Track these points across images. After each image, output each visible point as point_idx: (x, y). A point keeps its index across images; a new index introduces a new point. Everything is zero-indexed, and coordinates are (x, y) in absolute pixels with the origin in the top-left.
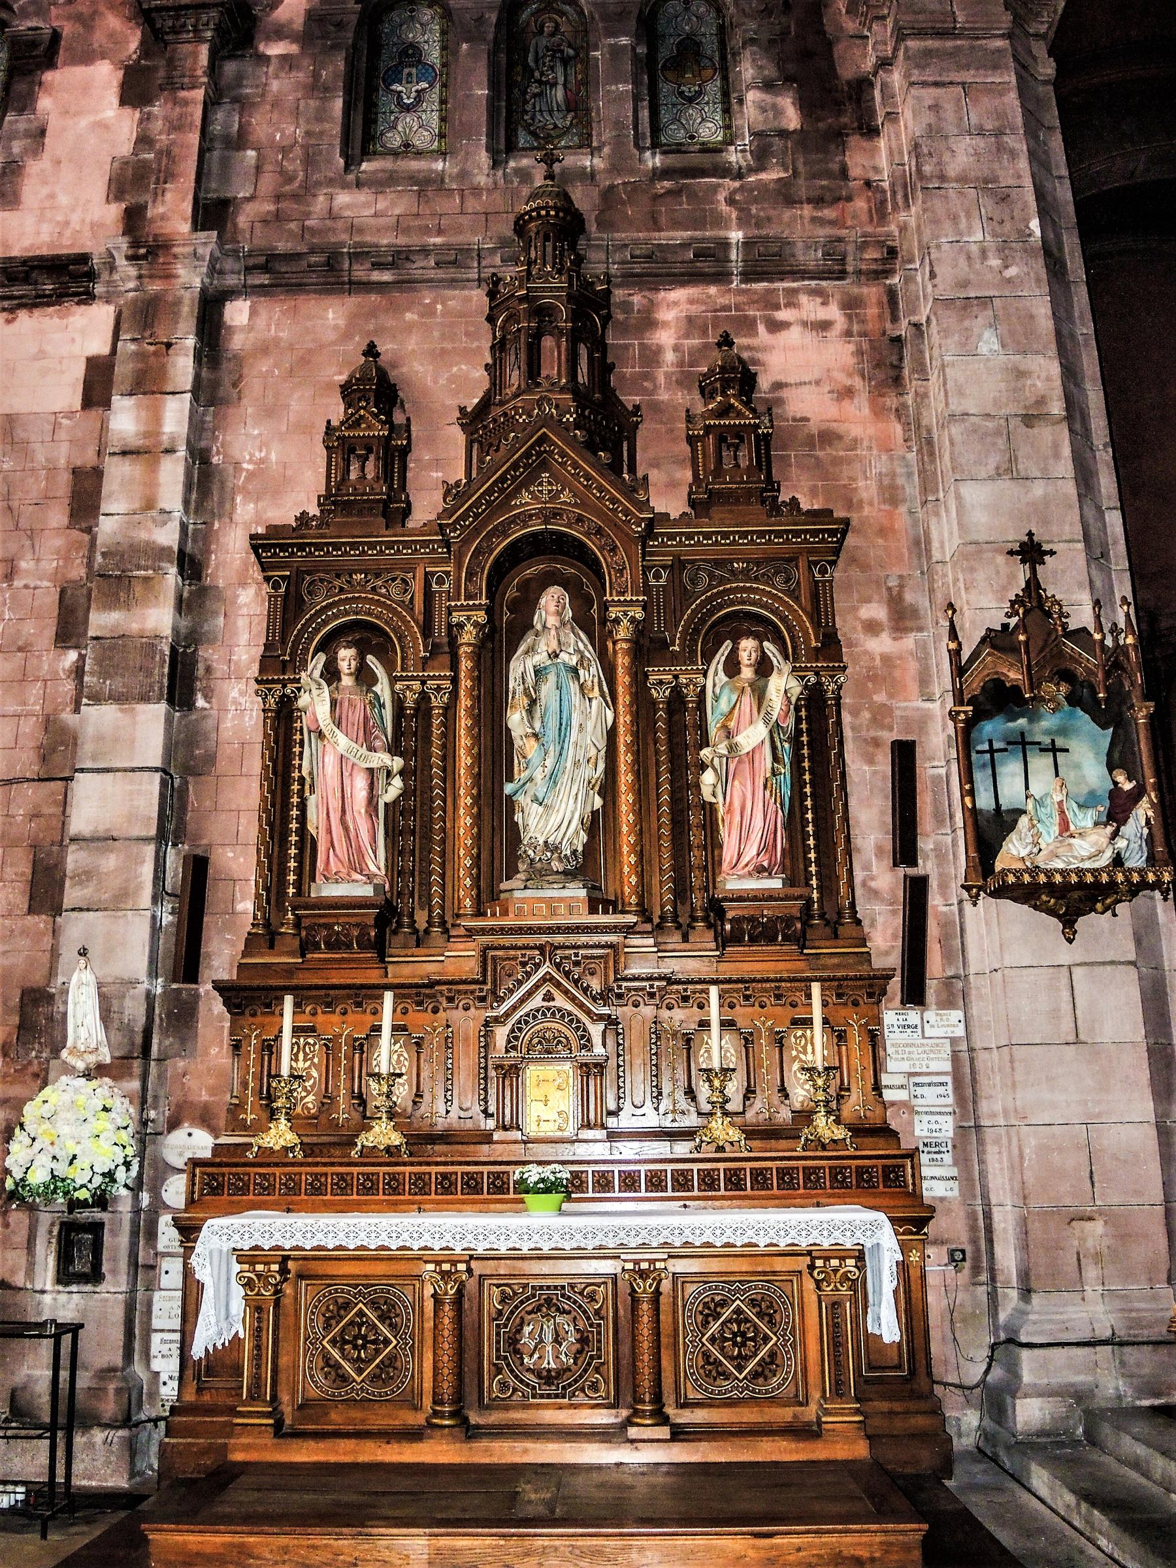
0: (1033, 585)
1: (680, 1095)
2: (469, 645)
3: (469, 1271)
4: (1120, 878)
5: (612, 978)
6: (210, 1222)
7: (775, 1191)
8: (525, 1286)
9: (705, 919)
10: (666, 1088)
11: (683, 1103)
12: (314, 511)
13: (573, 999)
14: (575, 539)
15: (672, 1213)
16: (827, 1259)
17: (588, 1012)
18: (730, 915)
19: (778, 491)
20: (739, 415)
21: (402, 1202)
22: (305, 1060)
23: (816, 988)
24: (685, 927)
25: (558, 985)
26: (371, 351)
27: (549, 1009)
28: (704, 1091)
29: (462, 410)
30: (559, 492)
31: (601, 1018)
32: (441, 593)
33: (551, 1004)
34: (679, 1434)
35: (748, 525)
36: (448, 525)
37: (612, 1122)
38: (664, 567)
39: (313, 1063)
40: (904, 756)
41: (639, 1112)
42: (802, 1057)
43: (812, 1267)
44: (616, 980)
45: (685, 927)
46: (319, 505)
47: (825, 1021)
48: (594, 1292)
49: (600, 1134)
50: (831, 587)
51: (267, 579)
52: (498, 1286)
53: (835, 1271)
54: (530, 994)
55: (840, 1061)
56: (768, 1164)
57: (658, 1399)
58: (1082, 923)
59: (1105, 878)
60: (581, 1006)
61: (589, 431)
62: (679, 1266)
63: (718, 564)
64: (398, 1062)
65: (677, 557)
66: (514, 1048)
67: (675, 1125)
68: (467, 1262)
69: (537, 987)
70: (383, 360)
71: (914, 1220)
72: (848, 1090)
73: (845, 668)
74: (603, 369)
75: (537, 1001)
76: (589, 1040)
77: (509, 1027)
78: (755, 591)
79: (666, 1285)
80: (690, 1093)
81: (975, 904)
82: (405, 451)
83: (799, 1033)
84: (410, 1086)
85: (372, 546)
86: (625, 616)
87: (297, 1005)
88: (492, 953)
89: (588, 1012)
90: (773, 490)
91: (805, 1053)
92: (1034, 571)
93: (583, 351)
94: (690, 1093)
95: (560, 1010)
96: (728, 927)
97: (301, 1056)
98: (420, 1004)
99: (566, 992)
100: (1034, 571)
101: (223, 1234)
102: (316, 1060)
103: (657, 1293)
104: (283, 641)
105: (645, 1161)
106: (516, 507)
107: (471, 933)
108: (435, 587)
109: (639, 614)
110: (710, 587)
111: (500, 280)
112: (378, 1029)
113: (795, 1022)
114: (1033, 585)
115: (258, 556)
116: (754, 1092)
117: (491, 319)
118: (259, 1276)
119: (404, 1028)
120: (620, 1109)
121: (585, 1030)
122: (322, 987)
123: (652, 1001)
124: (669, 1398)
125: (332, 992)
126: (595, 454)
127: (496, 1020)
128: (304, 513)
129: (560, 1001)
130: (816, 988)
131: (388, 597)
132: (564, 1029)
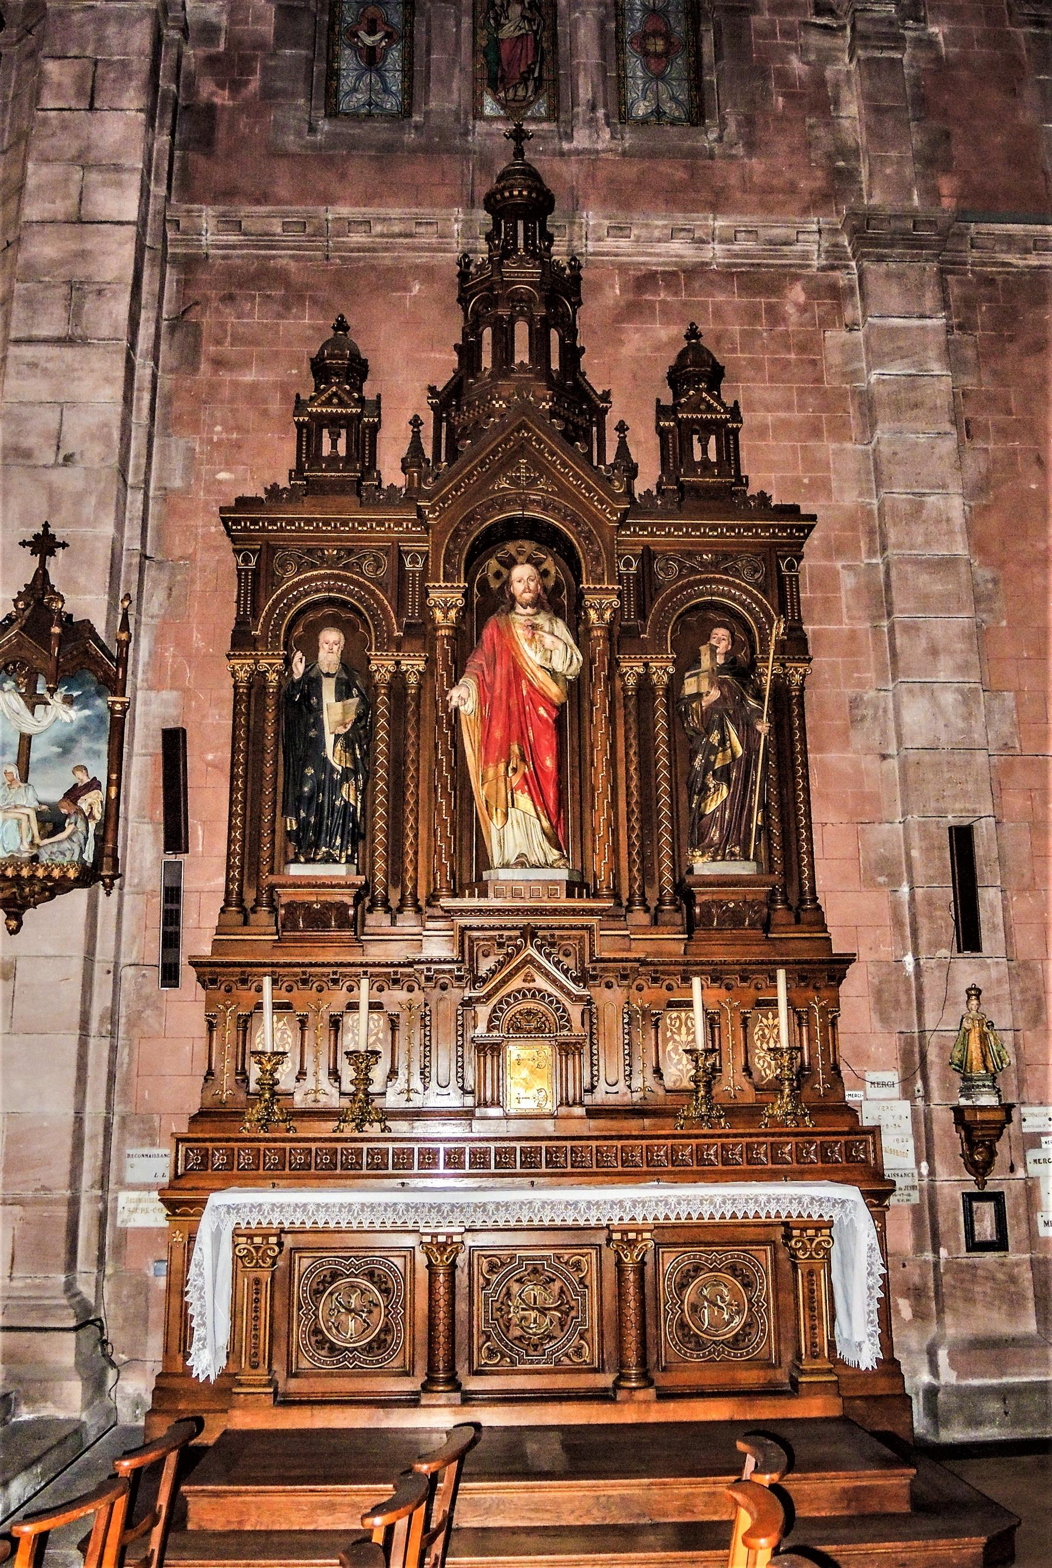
0: (42, 575)
1: (323, 1075)
2: (448, 627)
3: (280, 1244)
4: (40, 873)
5: (587, 960)
6: (215, 1199)
7: (441, 1170)
8: (513, 1257)
9: (672, 903)
10: (638, 1066)
11: (325, 1084)
12: (284, 483)
13: (554, 981)
14: (550, 525)
15: (520, 1188)
16: (804, 1229)
17: (569, 994)
18: (699, 899)
19: (747, 485)
20: (710, 409)
21: (662, 1173)
22: (688, 1034)
23: (781, 974)
24: (652, 910)
25: (539, 967)
26: (693, 333)
27: (529, 990)
28: (348, 1073)
29: (432, 389)
30: (536, 479)
31: (580, 998)
32: (414, 572)
33: (531, 985)
34: (665, 1396)
35: (312, 513)
36: (427, 507)
37: (587, 1099)
38: (254, 552)
39: (378, 1039)
40: (174, 742)
41: (614, 1089)
42: (676, 1037)
43: (609, 1240)
44: (591, 962)
45: (652, 910)
46: (290, 479)
47: (790, 1002)
48: (579, 1261)
49: (579, 1111)
50: (797, 581)
51: (237, 552)
52: (486, 1257)
53: (811, 1240)
54: (511, 975)
55: (801, 1041)
56: (513, 1144)
57: (451, 1367)
58: (28, 915)
59: (25, 873)
60: (562, 988)
61: (566, 420)
62: (470, 1240)
63: (690, 555)
64: (282, 1038)
65: (647, 548)
66: (495, 1027)
67: (411, 1104)
68: (279, 1236)
69: (517, 969)
70: (706, 342)
71: (878, 1192)
72: (720, 1071)
73: (810, 660)
74: (572, 354)
75: (517, 983)
76: (568, 1021)
77: (491, 1006)
78: (720, 582)
79: (462, 1259)
80: (335, 1074)
81: (108, 894)
82: (375, 428)
83: (674, 1015)
84: (294, 1063)
85: (344, 523)
86: (602, 604)
87: (275, 982)
88: (469, 933)
89: (569, 994)
90: (742, 484)
91: (679, 1034)
92: (42, 563)
93: (554, 335)
94: (335, 1074)
95: (540, 991)
96: (698, 910)
97: (684, 1029)
98: (655, 980)
99: (547, 974)
100: (42, 563)
101: (233, 1208)
102: (381, 1036)
103: (453, 1266)
104: (255, 615)
105: (496, 1139)
106: (494, 491)
107: (449, 914)
108: (408, 566)
109: (616, 604)
110: (680, 577)
111: (471, 261)
112: (259, 1006)
113: (759, 1004)
114: (42, 575)
115: (229, 530)
116: (305, 1074)
117: (463, 301)
118: (257, 1248)
119: (288, 1006)
120: (593, 1087)
121: (564, 1011)
122: (361, 965)
123: (625, 983)
124: (462, 1369)
125: (308, 970)
126: (572, 444)
127: (478, 1000)
128: (275, 486)
129: (541, 983)
130: (781, 974)
131: (362, 574)
132: (519, 1008)
